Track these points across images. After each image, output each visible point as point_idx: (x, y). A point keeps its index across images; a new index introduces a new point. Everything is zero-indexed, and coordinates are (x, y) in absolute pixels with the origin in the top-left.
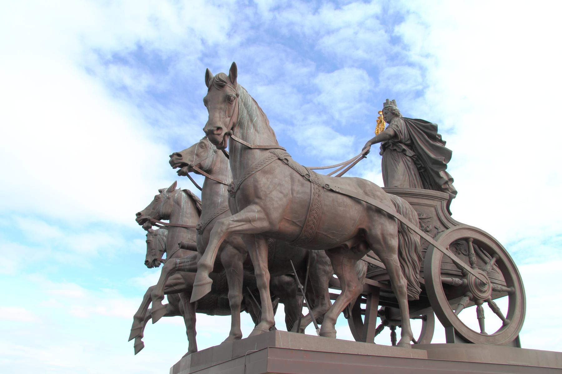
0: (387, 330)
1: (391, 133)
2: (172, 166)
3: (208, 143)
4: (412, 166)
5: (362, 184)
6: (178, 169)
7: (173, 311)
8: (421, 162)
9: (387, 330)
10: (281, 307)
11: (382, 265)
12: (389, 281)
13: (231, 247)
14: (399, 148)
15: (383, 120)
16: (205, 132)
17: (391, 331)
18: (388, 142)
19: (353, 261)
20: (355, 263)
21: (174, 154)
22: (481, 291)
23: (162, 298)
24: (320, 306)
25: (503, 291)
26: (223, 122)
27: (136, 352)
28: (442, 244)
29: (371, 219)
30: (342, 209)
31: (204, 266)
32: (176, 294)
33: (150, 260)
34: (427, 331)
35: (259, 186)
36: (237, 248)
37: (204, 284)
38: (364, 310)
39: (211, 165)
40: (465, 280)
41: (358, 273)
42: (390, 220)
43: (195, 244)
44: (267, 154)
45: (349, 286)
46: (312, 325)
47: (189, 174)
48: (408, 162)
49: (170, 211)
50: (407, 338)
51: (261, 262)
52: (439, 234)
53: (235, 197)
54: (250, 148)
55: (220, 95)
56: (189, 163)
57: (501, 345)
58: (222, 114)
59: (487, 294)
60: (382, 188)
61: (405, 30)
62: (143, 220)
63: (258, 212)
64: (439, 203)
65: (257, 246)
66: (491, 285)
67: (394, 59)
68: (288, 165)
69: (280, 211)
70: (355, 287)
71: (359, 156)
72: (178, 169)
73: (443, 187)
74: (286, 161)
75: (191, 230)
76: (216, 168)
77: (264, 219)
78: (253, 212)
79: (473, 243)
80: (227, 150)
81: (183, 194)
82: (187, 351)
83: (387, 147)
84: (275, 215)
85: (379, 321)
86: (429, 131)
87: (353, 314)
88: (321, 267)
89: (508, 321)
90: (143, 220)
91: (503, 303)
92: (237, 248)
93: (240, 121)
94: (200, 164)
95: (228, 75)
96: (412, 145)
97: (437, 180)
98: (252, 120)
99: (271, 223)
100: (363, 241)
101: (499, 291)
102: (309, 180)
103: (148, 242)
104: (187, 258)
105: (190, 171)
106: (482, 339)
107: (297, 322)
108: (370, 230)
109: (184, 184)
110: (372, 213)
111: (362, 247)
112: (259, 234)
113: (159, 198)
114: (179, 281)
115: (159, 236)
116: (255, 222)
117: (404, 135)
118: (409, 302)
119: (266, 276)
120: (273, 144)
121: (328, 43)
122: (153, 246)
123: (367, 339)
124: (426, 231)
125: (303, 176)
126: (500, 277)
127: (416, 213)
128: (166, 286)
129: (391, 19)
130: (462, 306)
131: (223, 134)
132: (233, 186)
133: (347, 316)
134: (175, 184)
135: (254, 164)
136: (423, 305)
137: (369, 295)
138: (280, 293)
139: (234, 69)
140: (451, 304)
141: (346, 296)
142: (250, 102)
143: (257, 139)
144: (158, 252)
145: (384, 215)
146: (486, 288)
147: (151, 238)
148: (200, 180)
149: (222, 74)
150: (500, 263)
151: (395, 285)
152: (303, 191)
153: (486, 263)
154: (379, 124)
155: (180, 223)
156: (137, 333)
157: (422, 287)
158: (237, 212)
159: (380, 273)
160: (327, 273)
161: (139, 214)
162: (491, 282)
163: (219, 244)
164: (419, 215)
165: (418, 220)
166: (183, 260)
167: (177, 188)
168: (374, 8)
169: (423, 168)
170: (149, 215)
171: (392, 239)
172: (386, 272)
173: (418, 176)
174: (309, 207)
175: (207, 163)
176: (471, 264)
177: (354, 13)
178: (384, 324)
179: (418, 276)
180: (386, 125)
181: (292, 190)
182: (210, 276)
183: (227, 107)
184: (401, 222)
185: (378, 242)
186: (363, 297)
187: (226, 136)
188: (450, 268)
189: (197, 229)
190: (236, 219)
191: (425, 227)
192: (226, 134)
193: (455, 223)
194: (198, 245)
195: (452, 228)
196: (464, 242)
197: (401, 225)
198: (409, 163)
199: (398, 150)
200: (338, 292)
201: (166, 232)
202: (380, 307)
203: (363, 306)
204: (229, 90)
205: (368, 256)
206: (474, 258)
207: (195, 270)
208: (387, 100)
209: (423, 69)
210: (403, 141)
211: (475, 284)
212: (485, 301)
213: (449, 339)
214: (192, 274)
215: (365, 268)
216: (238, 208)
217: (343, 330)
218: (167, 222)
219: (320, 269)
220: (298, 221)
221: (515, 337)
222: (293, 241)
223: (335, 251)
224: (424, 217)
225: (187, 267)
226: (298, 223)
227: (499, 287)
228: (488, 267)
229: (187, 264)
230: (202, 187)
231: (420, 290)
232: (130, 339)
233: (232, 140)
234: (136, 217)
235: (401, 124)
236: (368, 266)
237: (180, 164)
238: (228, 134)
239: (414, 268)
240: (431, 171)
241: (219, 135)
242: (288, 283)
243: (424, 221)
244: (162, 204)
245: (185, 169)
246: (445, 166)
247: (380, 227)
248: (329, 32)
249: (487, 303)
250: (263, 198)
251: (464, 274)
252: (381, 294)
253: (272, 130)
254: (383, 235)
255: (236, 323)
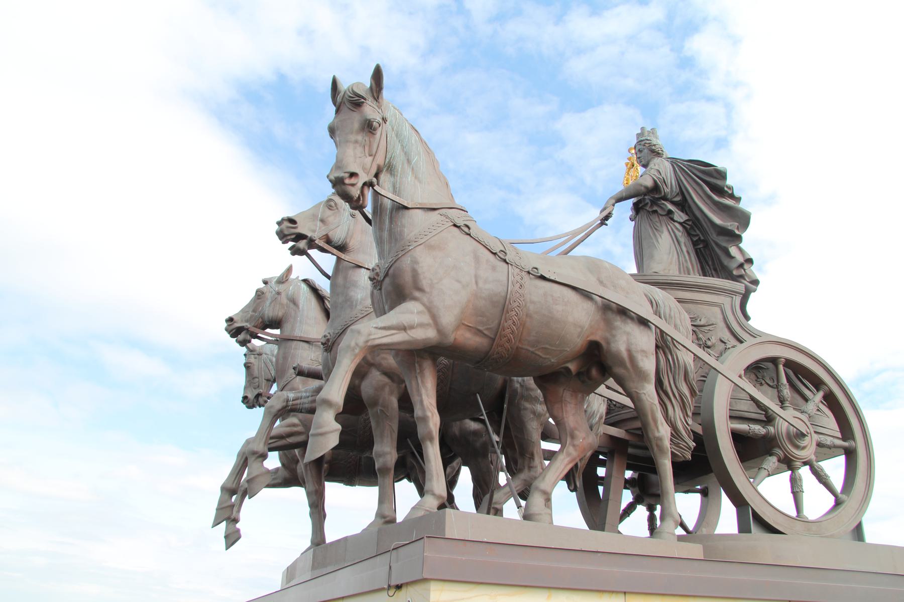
0: (641, 511)
1: (649, 183)
2: (281, 239)
3: (338, 200)
4: (683, 239)
5: (593, 265)
6: (291, 244)
7: (288, 478)
8: (698, 232)
9: (641, 511)
10: (465, 475)
11: (627, 401)
12: (639, 429)
13: (378, 373)
14: (662, 208)
15: (635, 163)
16: (331, 181)
17: (648, 513)
18: (644, 199)
19: (580, 395)
20: (583, 399)
21: (283, 220)
22: (797, 447)
23: (264, 457)
24: (526, 470)
25: (836, 447)
26: (361, 164)
27: (228, 546)
28: (732, 366)
29: (609, 324)
30: (559, 308)
31: (327, 403)
32: (292, 451)
33: (251, 396)
34: (707, 514)
35: (420, 271)
36: (388, 373)
37: (327, 434)
38: (602, 478)
39: (346, 238)
40: (771, 429)
41: (592, 416)
42: (642, 327)
43: (320, 367)
44: (434, 216)
45: (573, 437)
46: (512, 501)
47: (310, 252)
48: (676, 231)
49: (280, 314)
50: (670, 523)
51: (424, 397)
52: (728, 352)
53: (380, 289)
54: (406, 208)
55: (355, 120)
56: (309, 234)
57: (832, 536)
58: (359, 150)
59: (809, 452)
60: (632, 275)
61: (701, 45)
62: (237, 330)
63: (419, 313)
64: (729, 299)
65: (418, 371)
66: (815, 437)
67: (683, 91)
68: (469, 235)
69: (457, 311)
70: (584, 439)
71: (594, 221)
72: (291, 244)
73: (735, 273)
74: (466, 230)
75: (316, 346)
76: (352, 244)
77: (428, 325)
78: (409, 313)
79: (784, 366)
80: (368, 210)
81: (304, 286)
82: (309, 544)
83: (642, 208)
84: (448, 319)
85: (627, 497)
86: (712, 179)
87: (585, 482)
88: (528, 405)
89: (843, 497)
90: (237, 330)
91: (835, 468)
92: (388, 373)
93: (389, 163)
94: (327, 235)
95: (368, 86)
96: (684, 204)
97: (725, 261)
98: (409, 161)
99: (440, 331)
100: (596, 363)
101: (829, 447)
102: (505, 261)
103: (247, 366)
104: (306, 392)
105: (311, 247)
106: (799, 526)
107: (488, 496)
108: (608, 343)
109: (302, 268)
110: (610, 315)
111: (594, 372)
112: (420, 350)
113: (263, 293)
114: (295, 429)
115: (264, 356)
116: (413, 331)
117: (670, 187)
118: (674, 464)
119: (434, 421)
120: (444, 201)
121: (577, 67)
122: (256, 373)
123: (607, 526)
124: (706, 347)
125: (495, 254)
126: (830, 422)
127: (687, 316)
128: (272, 438)
129: (680, 28)
130: (766, 473)
131: (360, 184)
132: (378, 270)
133: (573, 488)
134: (289, 270)
135: (413, 234)
136: (699, 468)
137: (610, 454)
138: (455, 450)
139: (378, 75)
140: (746, 468)
141: (568, 454)
142: (407, 131)
143: (414, 191)
144: (264, 383)
145: (632, 319)
146: (806, 442)
147: (252, 359)
148: (328, 261)
149: (358, 84)
150: (831, 400)
151: (651, 436)
152: (495, 279)
153: (806, 400)
154: (630, 169)
155: (298, 333)
156: (228, 514)
157: (697, 437)
158: (385, 313)
159: (628, 416)
160: (538, 415)
161: (230, 320)
162: (815, 432)
163: (353, 367)
164: (693, 319)
165: (690, 328)
166: (299, 395)
167: (293, 276)
168: (655, 13)
169: (703, 241)
170: (247, 321)
171: (645, 359)
172: (635, 414)
173: (693, 255)
174: (504, 306)
175: (338, 236)
176: (782, 401)
177: (620, 22)
178: (638, 500)
179: (690, 421)
180: (641, 170)
181: (476, 277)
182: (337, 419)
183: (367, 139)
184: (661, 331)
185: (622, 363)
186: (601, 457)
187: (366, 188)
188: (745, 409)
189: (323, 344)
190: (381, 325)
191: (704, 339)
192: (365, 184)
193: (753, 334)
194: (324, 368)
195: (749, 340)
196: (770, 365)
197: (662, 337)
198: (679, 234)
199: (660, 211)
200: (555, 447)
201: (275, 348)
202: (628, 474)
203: (601, 472)
204: (370, 110)
205: (608, 387)
206: (787, 391)
207: (312, 411)
208: (642, 129)
209: (729, 107)
210: (669, 196)
211: (788, 434)
212: (805, 464)
213: (743, 528)
214: (309, 416)
215: (603, 409)
216: (386, 307)
217: (565, 508)
218: (277, 332)
219: (525, 409)
220: (487, 329)
221: (855, 524)
222: (478, 362)
223: (550, 379)
224: (702, 323)
225: (306, 406)
226: (486, 332)
227: (828, 441)
228: (811, 407)
229: (306, 400)
230: (330, 274)
231: (692, 444)
232: (216, 523)
233: (376, 193)
234: (225, 325)
235: (665, 168)
236: (609, 405)
237: (293, 237)
238: (369, 184)
239: (683, 408)
240: (714, 245)
241: (353, 185)
242: (475, 433)
243: (703, 329)
244: (268, 303)
245: (302, 244)
246: (739, 238)
247: (625, 338)
248: (580, 52)
249: (808, 467)
250: (427, 289)
251: (769, 419)
252: (630, 450)
253: (444, 177)
254: (629, 351)
255: (387, 498)
